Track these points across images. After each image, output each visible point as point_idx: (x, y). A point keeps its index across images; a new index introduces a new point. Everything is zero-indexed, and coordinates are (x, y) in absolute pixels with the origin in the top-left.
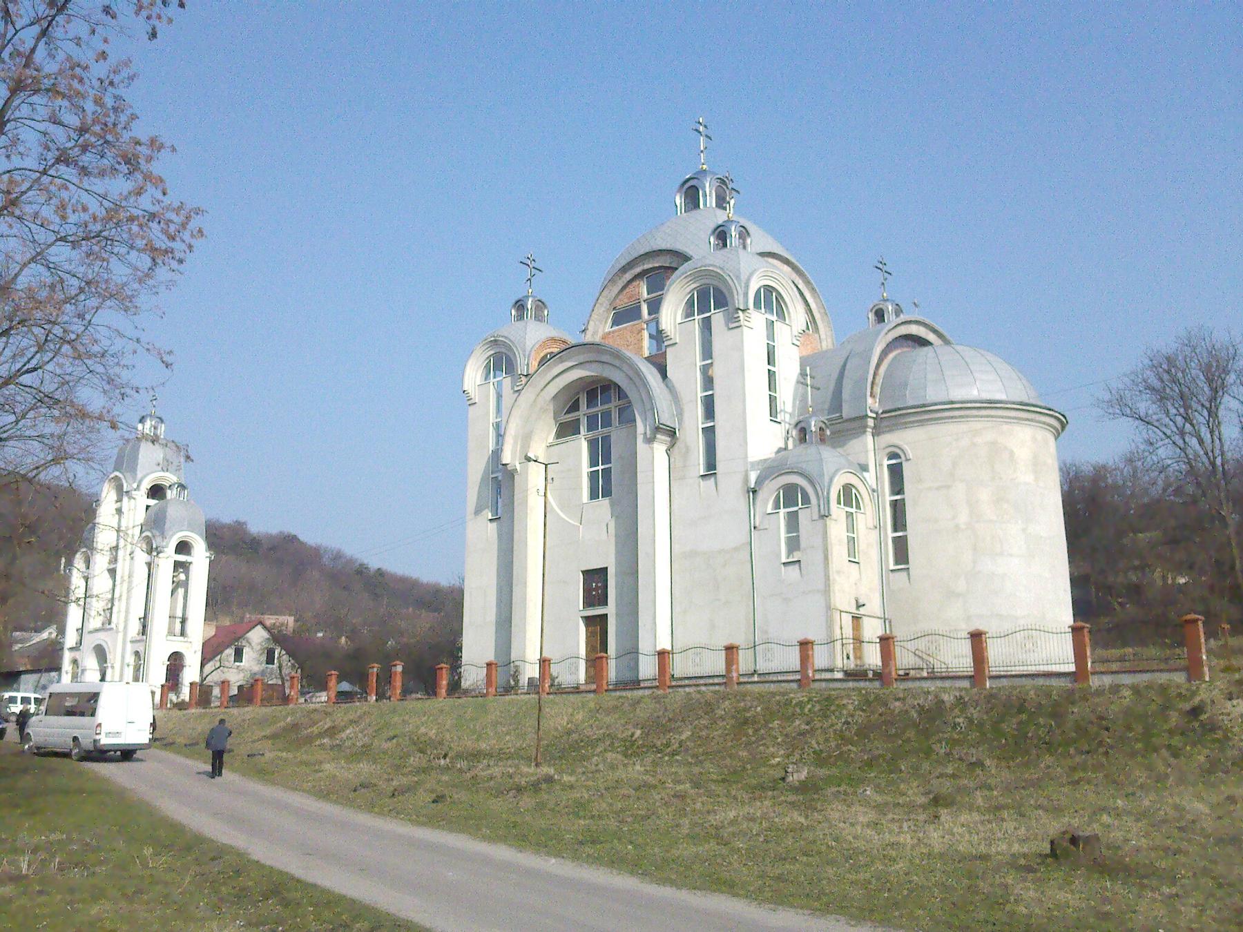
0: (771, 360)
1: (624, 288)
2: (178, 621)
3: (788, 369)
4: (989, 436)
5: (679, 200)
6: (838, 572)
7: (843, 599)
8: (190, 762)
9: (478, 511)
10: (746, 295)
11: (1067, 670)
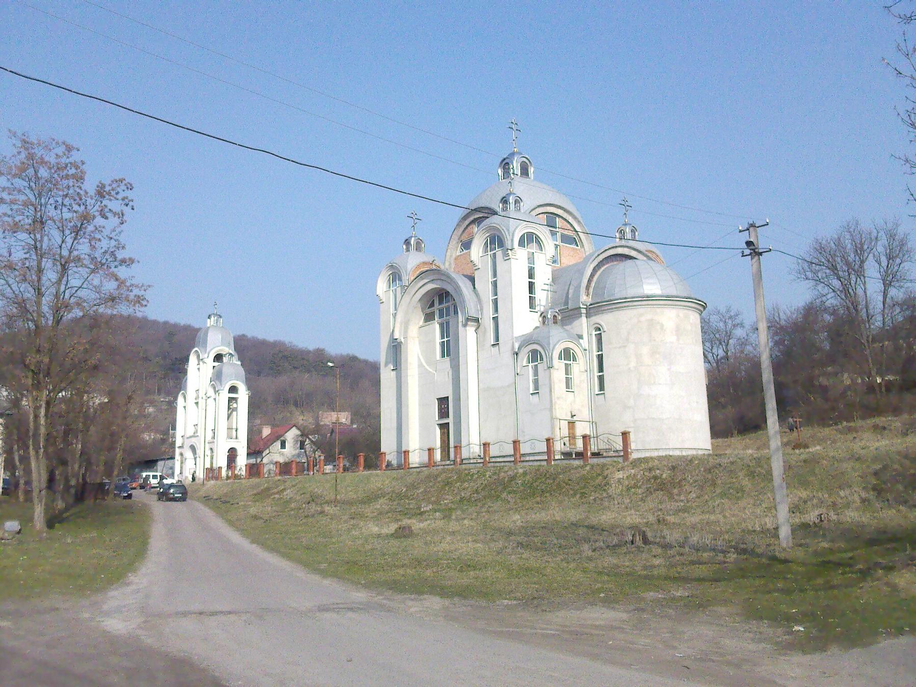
0: (531, 276)
1: (467, 226)
2: (234, 431)
3: (543, 276)
4: (649, 317)
5: (500, 172)
6: (558, 398)
7: (562, 411)
9: (386, 365)
10: (512, 240)
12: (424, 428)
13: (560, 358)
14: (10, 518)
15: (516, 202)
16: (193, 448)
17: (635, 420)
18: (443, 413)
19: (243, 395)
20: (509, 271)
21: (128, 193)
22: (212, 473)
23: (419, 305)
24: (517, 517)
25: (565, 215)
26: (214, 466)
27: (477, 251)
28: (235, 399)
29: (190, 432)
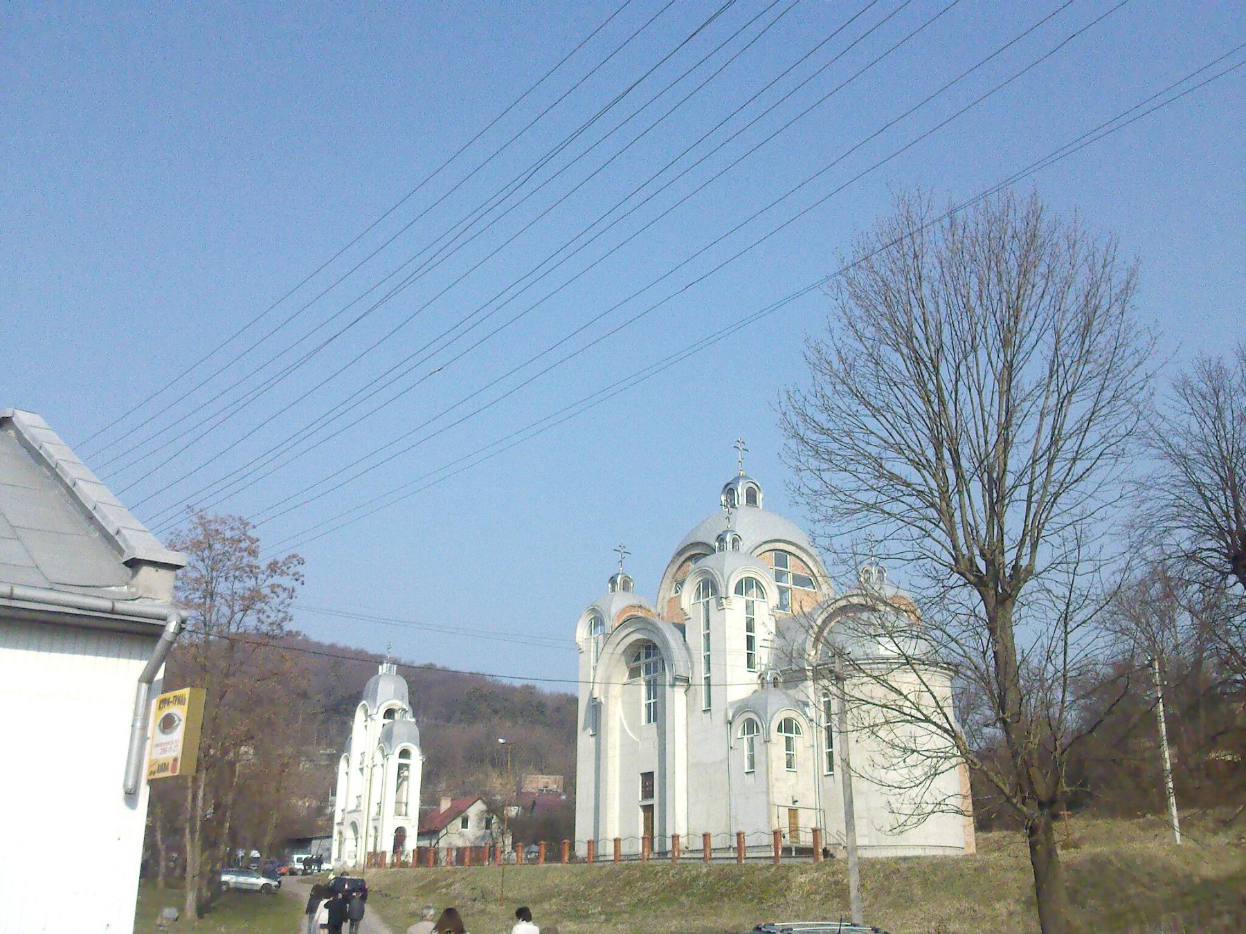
3: (765, 631)
7: (782, 793)
8: (188, 848)
9: (584, 729)
11: (768, 855)
12: (625, 810)
13: (779, 730)
14: (170, 905)
15: (734, 540)
16: (354, 826)
17: (869, 809)
18: (648, 792)
19: (416, 762)
20: (723, 623)
21: (300, 568)
22: (375, 858)
23: (623, 658)
24: (675, 922)
25: (798, 552)
26: (378, 850)
27: (688, 597)
28: (407, 766)
29: (352, 807)
